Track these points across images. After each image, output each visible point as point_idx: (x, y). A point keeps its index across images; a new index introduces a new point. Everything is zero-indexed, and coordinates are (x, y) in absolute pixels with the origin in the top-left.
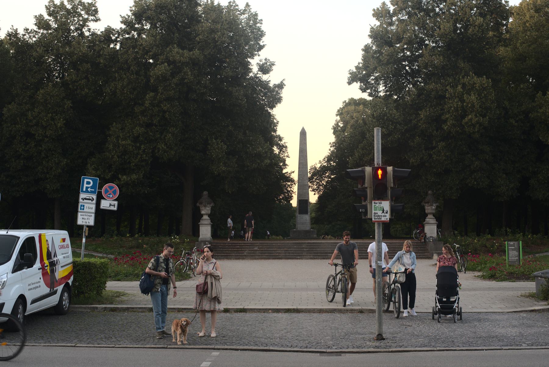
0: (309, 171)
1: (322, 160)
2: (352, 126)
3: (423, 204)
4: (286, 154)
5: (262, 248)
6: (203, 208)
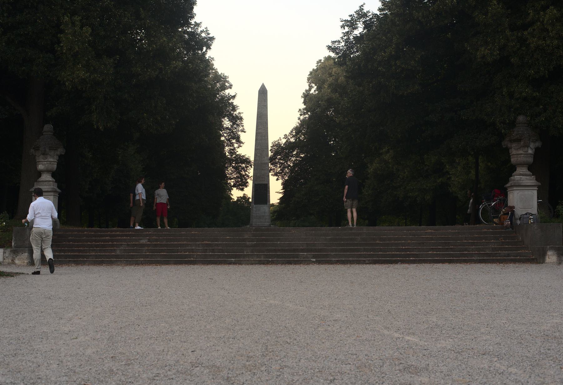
0: (270, 148)
1: (288, 134)
2: (330, 85)
3: (505, 143)
4: (241, 128)
5: (156, 240)
6: (40, 158)
